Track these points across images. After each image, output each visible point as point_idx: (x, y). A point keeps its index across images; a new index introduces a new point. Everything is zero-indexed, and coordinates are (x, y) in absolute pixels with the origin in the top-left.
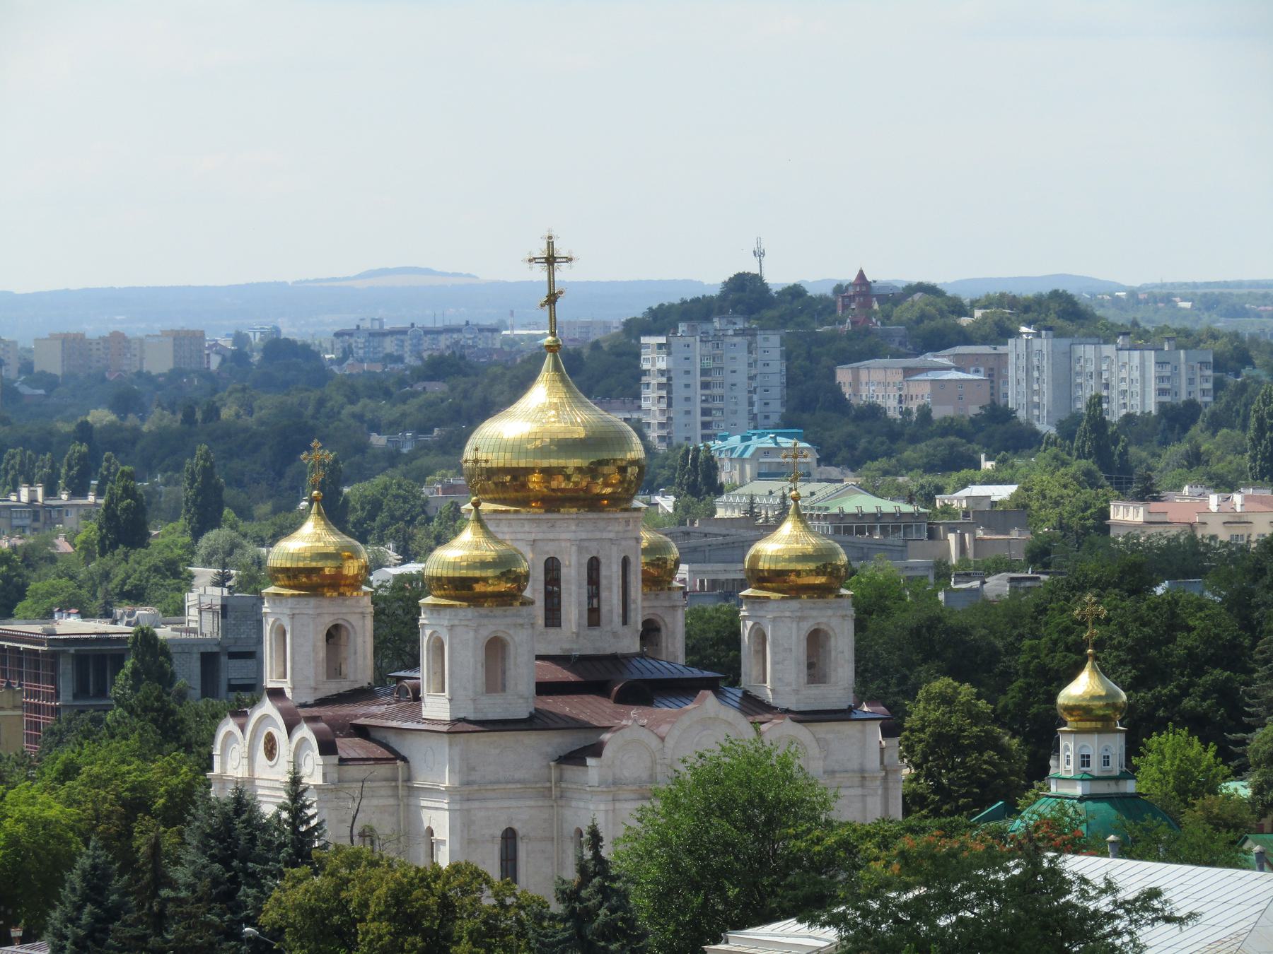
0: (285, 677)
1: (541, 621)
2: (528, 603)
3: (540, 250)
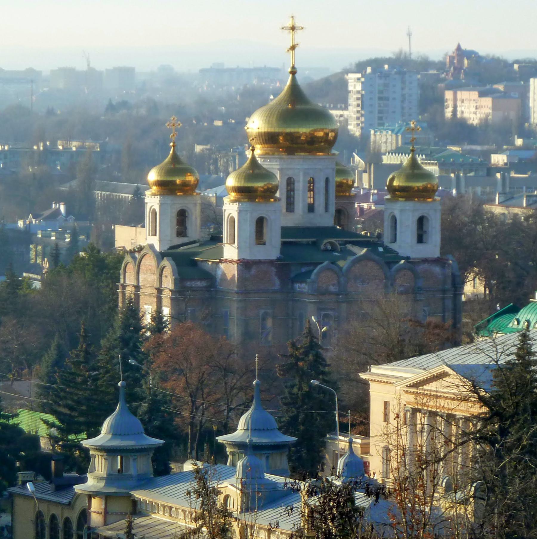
0: (156, 235)
1: (284, 210)
2: (277, 200)
3: (298, 24)
